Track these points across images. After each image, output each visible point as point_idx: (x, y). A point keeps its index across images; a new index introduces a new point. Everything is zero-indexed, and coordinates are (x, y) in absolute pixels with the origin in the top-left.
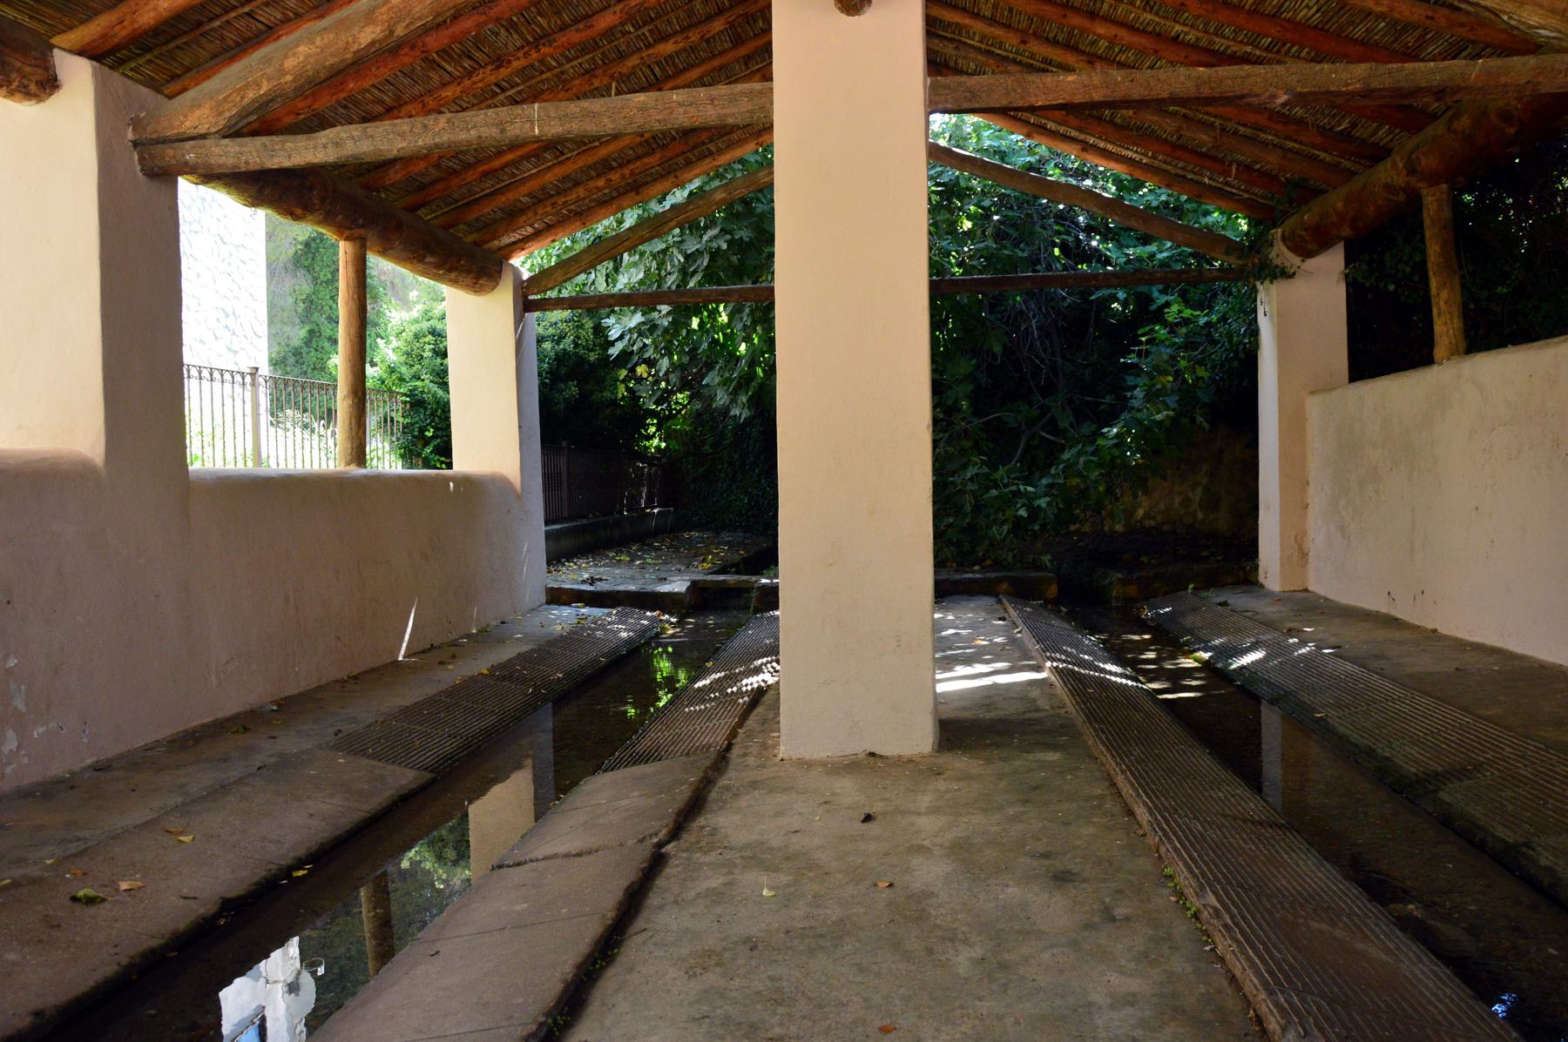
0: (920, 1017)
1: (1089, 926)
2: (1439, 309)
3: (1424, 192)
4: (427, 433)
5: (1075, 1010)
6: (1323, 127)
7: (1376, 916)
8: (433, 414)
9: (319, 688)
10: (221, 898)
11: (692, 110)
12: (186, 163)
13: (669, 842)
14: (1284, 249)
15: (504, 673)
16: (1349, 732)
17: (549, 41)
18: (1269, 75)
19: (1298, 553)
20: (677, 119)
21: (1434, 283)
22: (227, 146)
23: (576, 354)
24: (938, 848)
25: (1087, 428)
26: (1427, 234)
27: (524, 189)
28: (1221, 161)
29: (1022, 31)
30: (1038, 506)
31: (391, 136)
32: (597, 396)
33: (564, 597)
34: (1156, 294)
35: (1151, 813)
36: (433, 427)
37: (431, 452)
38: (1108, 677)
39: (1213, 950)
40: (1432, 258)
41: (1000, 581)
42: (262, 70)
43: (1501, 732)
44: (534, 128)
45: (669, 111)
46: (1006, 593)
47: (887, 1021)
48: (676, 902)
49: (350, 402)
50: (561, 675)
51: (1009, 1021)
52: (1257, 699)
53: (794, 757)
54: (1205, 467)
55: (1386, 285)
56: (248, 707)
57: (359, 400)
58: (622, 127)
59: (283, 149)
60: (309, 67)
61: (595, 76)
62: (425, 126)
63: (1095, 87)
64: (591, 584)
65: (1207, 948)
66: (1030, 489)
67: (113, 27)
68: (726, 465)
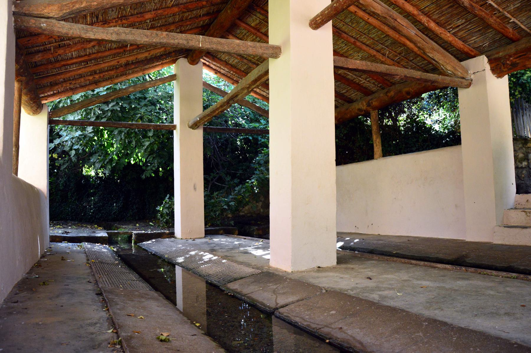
3: (371, 112)
11: (254, 49)
17: (126, 18)
20: (249, 51)
27: (63, 76)
33: (57, 239)
34: (260, 139)
40: (374, 130)
44: (199, 44)
45: (247, 48)
53: (296, 271)
58: (230, 50)
59: (92, 31)
63: (364, 65)
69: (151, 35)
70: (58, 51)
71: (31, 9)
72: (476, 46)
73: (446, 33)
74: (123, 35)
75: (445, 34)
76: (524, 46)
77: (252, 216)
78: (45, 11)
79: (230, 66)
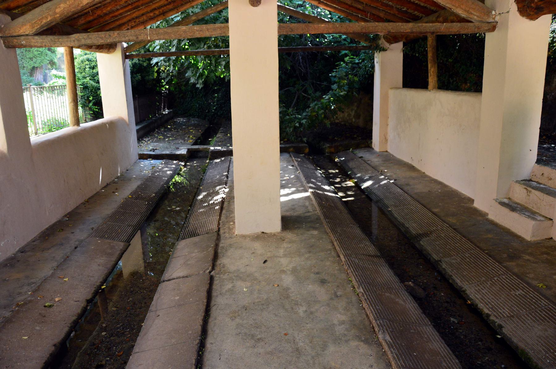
0: (293, 330)
1: (331, 299)
2: (431, 74)
4: (90, 98)
5: (330, 326)
6: (398, 8)
7: (402, 288)
8: (91, 91)
9: (77, 208)
10: (86, 300)
11: (201, 33)
12: (22, 45)
13: (212, 271)
14: (384, 41)
15: (137, 195)
16: (397, 217)
18: (383, 26)
19: (385, 140)
21: (429, 66)
22: (37, 39)
23: (139, 64)
24: (288, 271)
25: (318, 94)
26: (431, 24)
28: (365, 12)
30: (303, 123)
31: (98, 38)
32: (147, 78)
33: (145, 157)
35: (345, 258)
36: (92, 96)
37: (92, 105)
38: (326, 193)
39: (362, 306)
40: (429, 58)
41: (289, 147)
42: (48, 12)
43: (438, 220)
44: (148, 37)
46: (293, 152)
47: (286, 332)
48: (221, 294)
49: (73, 104)
50: (154, 195)
51: (315, 330)
52: (371, 200)
54: (356, 104)
55: (416, 54)
56: (58, 219)
57: (76, 103)
60: (65, 12)
62: (110, 36)
64: (153, 152)
65: (361, 305)
66: (300, 116)
68: (189, 92)
69: (105, 37)
70: (97, 12)
71: (11, 32)
74: (83, 40)
77: (345, 125)
78: (21, 31)
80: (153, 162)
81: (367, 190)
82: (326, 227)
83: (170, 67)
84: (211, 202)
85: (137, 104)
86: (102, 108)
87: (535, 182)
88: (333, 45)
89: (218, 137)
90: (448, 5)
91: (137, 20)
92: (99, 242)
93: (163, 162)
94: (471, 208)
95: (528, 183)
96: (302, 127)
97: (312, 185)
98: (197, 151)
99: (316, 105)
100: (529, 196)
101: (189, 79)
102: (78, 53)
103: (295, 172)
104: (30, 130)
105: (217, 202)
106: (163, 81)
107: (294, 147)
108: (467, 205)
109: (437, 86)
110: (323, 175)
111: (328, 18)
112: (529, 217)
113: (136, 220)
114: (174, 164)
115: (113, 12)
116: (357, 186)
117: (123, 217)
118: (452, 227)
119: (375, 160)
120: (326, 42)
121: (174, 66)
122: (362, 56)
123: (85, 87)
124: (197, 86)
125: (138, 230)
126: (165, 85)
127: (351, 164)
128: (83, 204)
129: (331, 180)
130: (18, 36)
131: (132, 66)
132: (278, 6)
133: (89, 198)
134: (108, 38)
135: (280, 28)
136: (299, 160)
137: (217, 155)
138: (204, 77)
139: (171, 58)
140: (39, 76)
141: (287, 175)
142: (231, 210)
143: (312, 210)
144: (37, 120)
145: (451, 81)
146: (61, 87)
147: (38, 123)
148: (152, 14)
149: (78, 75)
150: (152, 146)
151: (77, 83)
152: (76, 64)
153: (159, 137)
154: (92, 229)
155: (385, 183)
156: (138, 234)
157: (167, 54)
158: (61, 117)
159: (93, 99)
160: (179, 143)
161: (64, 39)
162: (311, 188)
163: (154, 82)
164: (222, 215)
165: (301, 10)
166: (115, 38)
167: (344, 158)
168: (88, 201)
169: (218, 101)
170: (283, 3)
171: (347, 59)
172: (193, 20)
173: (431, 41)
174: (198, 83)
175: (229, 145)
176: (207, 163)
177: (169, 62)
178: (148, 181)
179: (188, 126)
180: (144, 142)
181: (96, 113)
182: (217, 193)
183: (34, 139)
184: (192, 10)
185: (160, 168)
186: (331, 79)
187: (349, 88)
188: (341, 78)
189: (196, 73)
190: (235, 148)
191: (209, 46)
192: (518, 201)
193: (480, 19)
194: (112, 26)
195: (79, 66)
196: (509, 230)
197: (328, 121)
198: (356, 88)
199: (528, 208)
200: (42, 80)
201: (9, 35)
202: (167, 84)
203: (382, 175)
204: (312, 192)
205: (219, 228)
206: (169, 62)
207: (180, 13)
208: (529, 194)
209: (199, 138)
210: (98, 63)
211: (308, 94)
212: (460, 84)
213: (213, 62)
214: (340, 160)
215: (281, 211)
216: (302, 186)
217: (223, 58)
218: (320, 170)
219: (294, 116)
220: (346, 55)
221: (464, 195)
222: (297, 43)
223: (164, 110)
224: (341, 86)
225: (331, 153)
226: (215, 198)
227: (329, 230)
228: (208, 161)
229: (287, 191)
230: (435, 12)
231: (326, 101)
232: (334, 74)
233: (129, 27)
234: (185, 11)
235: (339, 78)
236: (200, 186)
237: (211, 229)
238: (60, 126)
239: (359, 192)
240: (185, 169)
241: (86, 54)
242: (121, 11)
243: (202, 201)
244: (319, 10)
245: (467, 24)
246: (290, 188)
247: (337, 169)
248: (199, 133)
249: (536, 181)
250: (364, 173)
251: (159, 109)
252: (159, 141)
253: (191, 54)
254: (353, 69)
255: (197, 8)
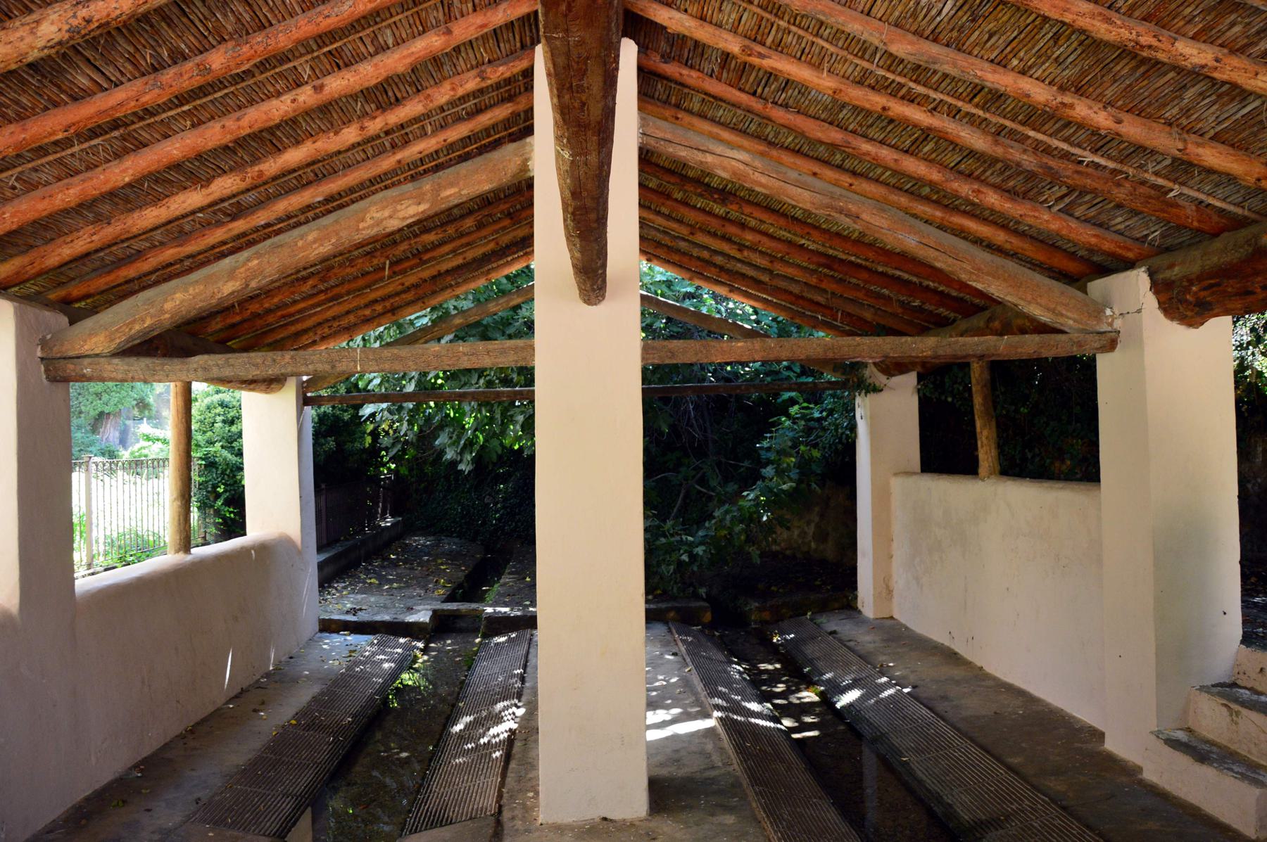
6: (903, 302)
8: (223, 473)
9: (166, 746)
11: (474, 359)
14: (875, 370)
15: (309, 719)
16: (924, 778)
19: (885, 591)
21: (978, 424)
23: (333, 415)
25: (732, 487)
26: (976, 338)
28: (832, 309)
29: (691, 225)
30: (697, 554)
32: (348, 446)
33: (333, 626)
38: (753, 720)
41: (668, 610)
52: (859, 736)
59: (163, 370)
61: (375, 257)
62: (274, 360)
63: (756, 351)
66: (690, 538)
67: (24, 267)
72: (1138, 236)
73: (1036, 214)
75: (1036, 217)
76: (1215, 259)
78: (86, 347)
79: (665, 249)
80: (351, 638)
81: (850, 712)
82: (754, 805)
83: (402, 425)
84: (482, 741)
85: (323, 504)
86: (244, 510)
87: (1245, 688)
88: (763, 380)
89: (505, 584)
90: (1008, 298)
91: (336, 324)
92: (211, 834)
93: (374, 639)
94: (1100, 753)
95: (1227, 690)
96: (697, 564)
97: (720, 701)
98: (455, 615)
99: (727, 512)
100: (1236, 723)
101: (442, 452)
102: (200, 389)
103: (679, 669)
104: (76, 556)
105: (497, 740)
106: (383, 453)
107: (678, 610)
108: (1089, 746)
109: (998, 468)
110: (745, 676)
111: (748, 321)
112: (1243, 777)
113: (302, 782)
114: (400, 646)
115: (286, 305)
116: (826, 701)
117: (272, 773)
118: (1055, 803)
119: (866, 640)
120: (747, 373)
121: (410, 423)
122: (828, 402)
123: (210, 464)
124: (459, 468)
125: (308, 805)
126: (388, 462)
127: (810, 650)
128: (181, 737)
129: (764, 688)
130: (78, 357)
131: (316, 420)
132: (642, 297)
133: (198, 724)
134: (269, 366)
135: (646, 349)
136: (690, 639)
137: (499, 625)
138: (476, 447)
139: (405, 405)
140: (110, 433)
141: (661, 677)
142: (530, 760)
143: (720, 764)
144: (94, 534)
145: (1029, 455)
146: (156, 463)
147: (97, 542)
148: (367, 312)
149: (198, 437)
150: (352, 603)
151: (193, 454)
152: (193, 412)
153: (369, 581)
154: (198, 801)
155: (891, 695)
156: (306, 820)
157: (395, 398)
158: (151, 529)
159: (225, 491)
160: (414, 596)
161: (175, 365)
162: (718, 707)
163: (364, 456)
164: (509, 774)
165: (692, 305)
166: (284, 366)
167: (792, 636)
168: (192, 731)
169: (505, 500)
170: (653, 289)
171: (794, 410)
172: (456, 326)
173: (977, 373)
174: (461, 461)
175: (528, 603)
176: (475, 645)
177: (399, 414)
178: (339, 684)
179: (437, 556)
180: (334, 591)
181: (230, 522)
182: (498, 719)
183: (84, 582)
184: (455, 304)
185: (367, 653)
186: (759, 455)
187: (801, 474)
188: (781, 453)
189: (459, 438)
190: (544, 609)
191: (490, 380)
192: (1211, 736)
193: (1081, 326)
194: (282, 335)
195: (202, 417)
196: (1199, 809)
197: (754, 548)
198: (817, 475)
199: (1237, 753)
200: (117, 441)
201: (59, 355)
202: (393, 460)
203: (884, 675)
204: (721, 719)
205: (500, 807)
206: (399, 414)
207: (428, 310)
208: (1235, 718)
209: (460, 586)
210: (244, 412)
211: (709, 488)
212: (1048, 461)
213: (498, 416)
214: (785, 639)
215: (648, 765)
216: (698, 702)
217: (518, 406)
218: (739, 665)
219: (678, 538)
220: (793, 402)
221: (1079, 721)
222: (684, 377)
223: (384, 519)
224: (783, 471)
225: (764, 622)
226: (493, 731)
227: (761, 814)
228: (478, 640)
229: (661, 715)
230: (983, 309)
231: (749, 504)
232: (765, 444)
233: (317, 338)
234: (441, 305)
235: (779, 453)
236: (458, 699)
237: (482, 808)
238: (145, 550)
239: (830, 717)
240: (426, 658)
241: (218, 392)
242: (302, 305)
243: (460, 735)
244: (731, 305)
245: (1053, 336)
246: (667, 707)
247: (778, 661)
248: (461, 575)
249: (1249, 686)
250: (839, 671)
251: (372, 517)
252: (368, 589)
253: (451, 398)
254: (808, 431)
255: (465, 299)
